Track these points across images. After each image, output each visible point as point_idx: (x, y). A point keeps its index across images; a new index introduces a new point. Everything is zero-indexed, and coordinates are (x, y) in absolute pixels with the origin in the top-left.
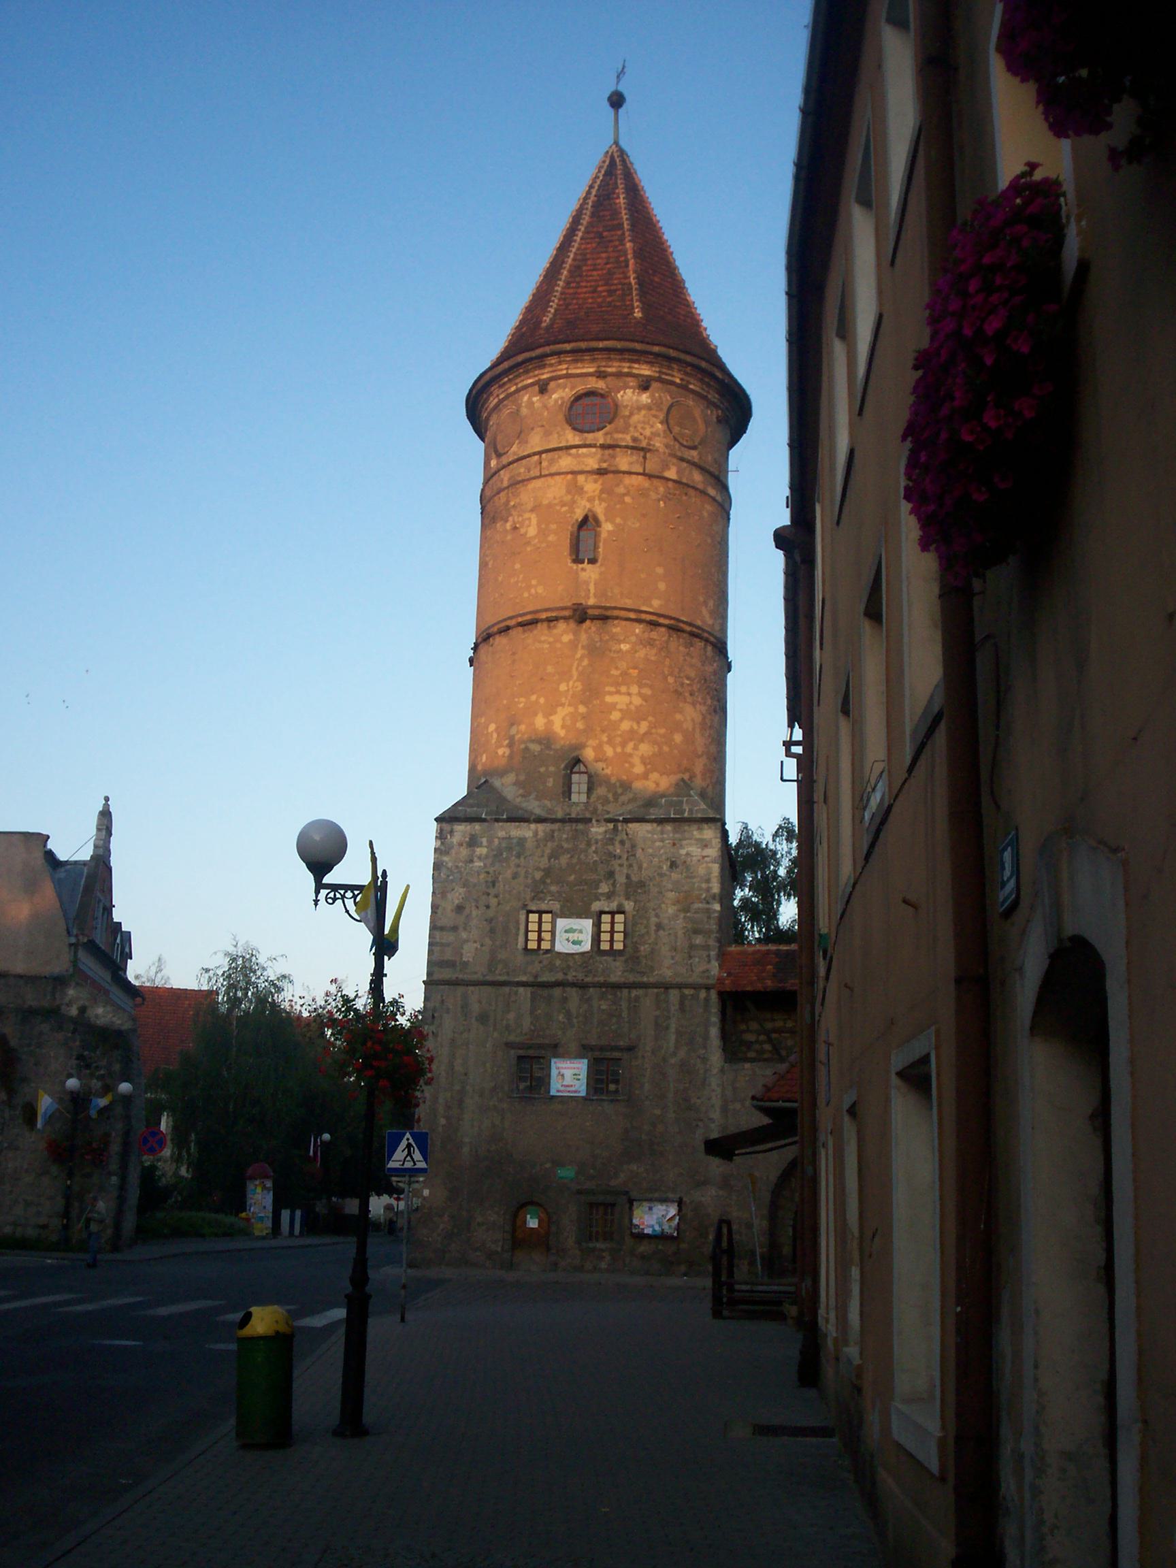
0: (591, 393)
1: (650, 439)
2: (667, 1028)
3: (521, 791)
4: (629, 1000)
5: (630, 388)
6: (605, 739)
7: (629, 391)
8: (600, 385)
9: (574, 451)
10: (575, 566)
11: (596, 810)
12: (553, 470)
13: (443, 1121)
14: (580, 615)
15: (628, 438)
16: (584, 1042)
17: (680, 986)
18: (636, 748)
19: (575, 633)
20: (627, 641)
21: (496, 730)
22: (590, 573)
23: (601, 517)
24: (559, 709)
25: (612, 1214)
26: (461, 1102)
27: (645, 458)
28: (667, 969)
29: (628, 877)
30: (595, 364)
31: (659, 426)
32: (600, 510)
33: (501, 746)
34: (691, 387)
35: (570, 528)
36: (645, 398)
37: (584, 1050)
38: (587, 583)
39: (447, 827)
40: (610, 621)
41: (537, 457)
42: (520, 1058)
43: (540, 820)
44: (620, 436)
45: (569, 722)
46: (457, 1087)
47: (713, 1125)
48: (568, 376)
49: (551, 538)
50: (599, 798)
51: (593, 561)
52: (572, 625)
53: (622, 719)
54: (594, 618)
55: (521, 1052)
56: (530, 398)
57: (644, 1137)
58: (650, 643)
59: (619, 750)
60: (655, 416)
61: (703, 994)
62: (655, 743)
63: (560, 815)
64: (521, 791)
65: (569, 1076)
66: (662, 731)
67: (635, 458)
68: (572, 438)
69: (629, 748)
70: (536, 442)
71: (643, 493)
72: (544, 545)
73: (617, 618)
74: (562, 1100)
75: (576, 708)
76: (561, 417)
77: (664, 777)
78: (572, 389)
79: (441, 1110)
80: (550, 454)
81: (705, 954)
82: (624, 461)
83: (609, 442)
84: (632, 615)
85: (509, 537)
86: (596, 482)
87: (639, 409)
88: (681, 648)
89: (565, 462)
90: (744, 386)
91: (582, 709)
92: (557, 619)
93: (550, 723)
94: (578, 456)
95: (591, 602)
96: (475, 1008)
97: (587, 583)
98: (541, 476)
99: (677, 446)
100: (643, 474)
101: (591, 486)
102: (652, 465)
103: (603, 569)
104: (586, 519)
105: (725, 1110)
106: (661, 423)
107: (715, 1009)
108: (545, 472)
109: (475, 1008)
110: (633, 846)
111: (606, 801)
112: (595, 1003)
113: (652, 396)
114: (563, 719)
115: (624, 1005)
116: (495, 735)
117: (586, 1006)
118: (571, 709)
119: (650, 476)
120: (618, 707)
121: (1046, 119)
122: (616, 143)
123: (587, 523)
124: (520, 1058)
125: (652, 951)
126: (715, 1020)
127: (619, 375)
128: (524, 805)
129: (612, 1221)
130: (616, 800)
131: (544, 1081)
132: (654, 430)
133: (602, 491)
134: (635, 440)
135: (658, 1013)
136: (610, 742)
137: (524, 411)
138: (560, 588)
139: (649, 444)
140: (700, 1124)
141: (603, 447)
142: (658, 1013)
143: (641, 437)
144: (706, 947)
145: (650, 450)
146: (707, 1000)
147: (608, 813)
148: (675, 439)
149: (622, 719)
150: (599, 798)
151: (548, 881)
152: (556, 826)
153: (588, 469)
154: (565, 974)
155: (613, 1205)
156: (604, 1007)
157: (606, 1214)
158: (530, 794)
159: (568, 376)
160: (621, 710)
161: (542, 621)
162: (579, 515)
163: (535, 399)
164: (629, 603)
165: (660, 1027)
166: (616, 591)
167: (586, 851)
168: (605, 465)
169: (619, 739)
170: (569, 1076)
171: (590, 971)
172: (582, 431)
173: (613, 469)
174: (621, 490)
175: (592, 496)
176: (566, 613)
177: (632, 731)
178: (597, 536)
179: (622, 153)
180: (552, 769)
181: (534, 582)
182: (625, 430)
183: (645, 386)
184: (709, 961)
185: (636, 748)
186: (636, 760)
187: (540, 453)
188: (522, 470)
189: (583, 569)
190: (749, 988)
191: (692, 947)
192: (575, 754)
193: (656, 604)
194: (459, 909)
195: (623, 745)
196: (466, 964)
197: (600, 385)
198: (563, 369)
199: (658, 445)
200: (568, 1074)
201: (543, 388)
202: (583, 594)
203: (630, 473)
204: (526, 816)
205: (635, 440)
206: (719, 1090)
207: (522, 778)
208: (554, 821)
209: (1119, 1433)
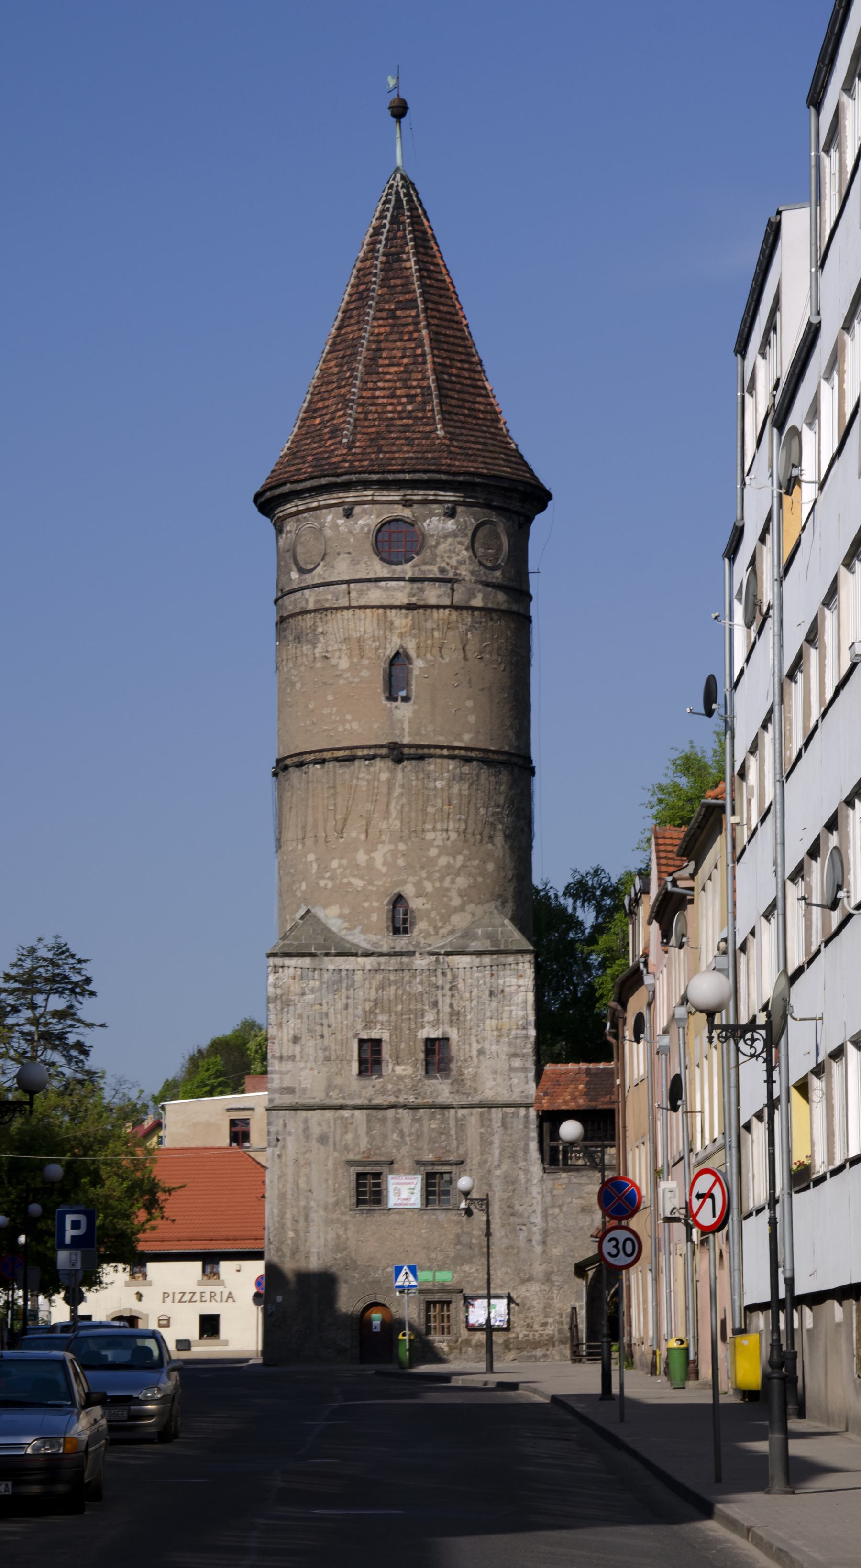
0: (397, 520)
1: (456, 568)
2: (491, 1143)
3: (346, 925)
4: (457, 1120)
5: (435, 515)
6: (424, 875)
7: (435, 519)
8: (407, 513)
9: (383, 584)
10: (389, 704)
11: (418, 943)
13: (291, 1234)
14: (397, 754)
15: (435, 569)
16: (417, 1158)
18: (453, 882)
19: (393, 772)
20: (441, 775)
21: (317, 859)
22: (404, 711)
23: (412, 653)
24: (380, 846)
25: (448, 1311)
26: (307, 1217)
27: (453, 590)
28: (491, 1088)
29: (451, 1006)
30: (402, 493)
31: (465, 553)
32: (411, 646)
33: (323, 878)
34: (494, 504)
35: (383, 665)
36: (450, 524)
38: (401, 721)
40: (427, 761)
41: (344, 586)
42: (360, 1176)
44: (427, 567)
45: (390, 859)
46: (302, 1203)
47: (535, 1229)
48: (374, 502)
49: (365, 673)
50: (421, 932)
51: (406, 699)
52: (390, 763)
53: (439, 855)
54: (410, 758)
55: (360, 1169)
56: (333, 521)
57: (474, 1241)
58: (462, 778)
59: (437, 885)
60: (460, 543)
62: (470, 875)
63: (385, 949)
64: (346, 925)
65: (404, 1191)
66: (476, 863)
67: (442, 590)
68: (380, 569)
69: (447, 883)
70: (342, 569)
71: (449, 626)
72: (356, 680)
73: (431, 756)
74: (401, 1212)
75: (397, 846)
76: (368, 546)
77: (479, 906)
78: (378, 516)
79: (289, 1223)
80: (359, 585)
81: (522, 1075)
82: (433, 594)
83: (418, 575)
84: (445, 752)
85: (318, 665)
86: (406, 616)
87: (445, 537)
88: (492, 779)
89: (375, 595)
90: (534, 661)
91: (402, 847)
92: (374, 757)
93: (371, 860)
94: (387, 589)
95: (406, 740)
96: (316, 1131)
97: (401, 721)
98: (348, 608)
99: (483, 570)
100: (453, 607)
101: (401, 620)
102: (459, 597)
103: (416, 707)
104: (397, 654)
105: (545, 1215)
106: (467, 549)
107: (533, 1125)
108: (354, 603)
109: (316, 1131)
110: (454, 977)
111: (428, 935)
112: (425, 1122)
113: (457, 523)
114: (384, 855)
115: (452, 1123)
116: (315, 866)
117: (417, 1125)
118: (391, 847)
120: (436, 843)
124: (360, 1176)
125: (476, 1075)
128: (349, 938)
129: (448, 1316)
130: (437, 933)
132: (459, 558)
133: (413, 627)
134: (442, 570)
135: (482, 1130)
136: (429, 878)
137: (328, 532)
138: (375, 726)
139: (456, 574)
140: (524, 1228)
141: (412, 580)
142: (482, 1130)
143: (448, 567)
144: (525, 1069)
145: (457, 581)
146: (527, 1116)
147: (430, 945)
148: (481, 564)
149: (439, 855)
150: (421, 932)
151: (378, 1011)
152: (383, 959)
153: (398, 603)
154: (397, 1097)
155: (449, 1303)
156: (433, 1126)
157: (442, 1310)
158: (355, 927)
160: (438, 846)
161: (361, 758)
162: (390, 652)
163: (340, 522)
164: (441, 740)
165: (485, 1142)
166: (430, 728)
167: (410, 982)
168: (414, 600)
169: (437, 875)
171: (419, 1094)
172: (390, 563)
173: (422, 603)
174: (429, 625)
175: (400, 634)
176: (384, 751)
177: (449, 866)
178: (409, 672)
180: (376, 904)
181: (349, 717)
182: (432, 562)
183: (451, 514)
184: (527, 1083)
185: (453, 882)
186: (454, 894)
187: (348, 582)
188: (330, 597)
189: (396, 707)
190: (564, 1108)
191: (512, 1069)
192: (396, 891)
193: (467, 739)
195: (442, 879)
196: (304, 1090)
197: (407, 513)
199: (464, 573)
200: (405, 1194)
202: (397, 732)
203: (438, 607)
204: (353, 951)
205: (442, 570)
206: (539, 1197)
207: (346, 911)
208: (381, 954)
209: (373, 1037)
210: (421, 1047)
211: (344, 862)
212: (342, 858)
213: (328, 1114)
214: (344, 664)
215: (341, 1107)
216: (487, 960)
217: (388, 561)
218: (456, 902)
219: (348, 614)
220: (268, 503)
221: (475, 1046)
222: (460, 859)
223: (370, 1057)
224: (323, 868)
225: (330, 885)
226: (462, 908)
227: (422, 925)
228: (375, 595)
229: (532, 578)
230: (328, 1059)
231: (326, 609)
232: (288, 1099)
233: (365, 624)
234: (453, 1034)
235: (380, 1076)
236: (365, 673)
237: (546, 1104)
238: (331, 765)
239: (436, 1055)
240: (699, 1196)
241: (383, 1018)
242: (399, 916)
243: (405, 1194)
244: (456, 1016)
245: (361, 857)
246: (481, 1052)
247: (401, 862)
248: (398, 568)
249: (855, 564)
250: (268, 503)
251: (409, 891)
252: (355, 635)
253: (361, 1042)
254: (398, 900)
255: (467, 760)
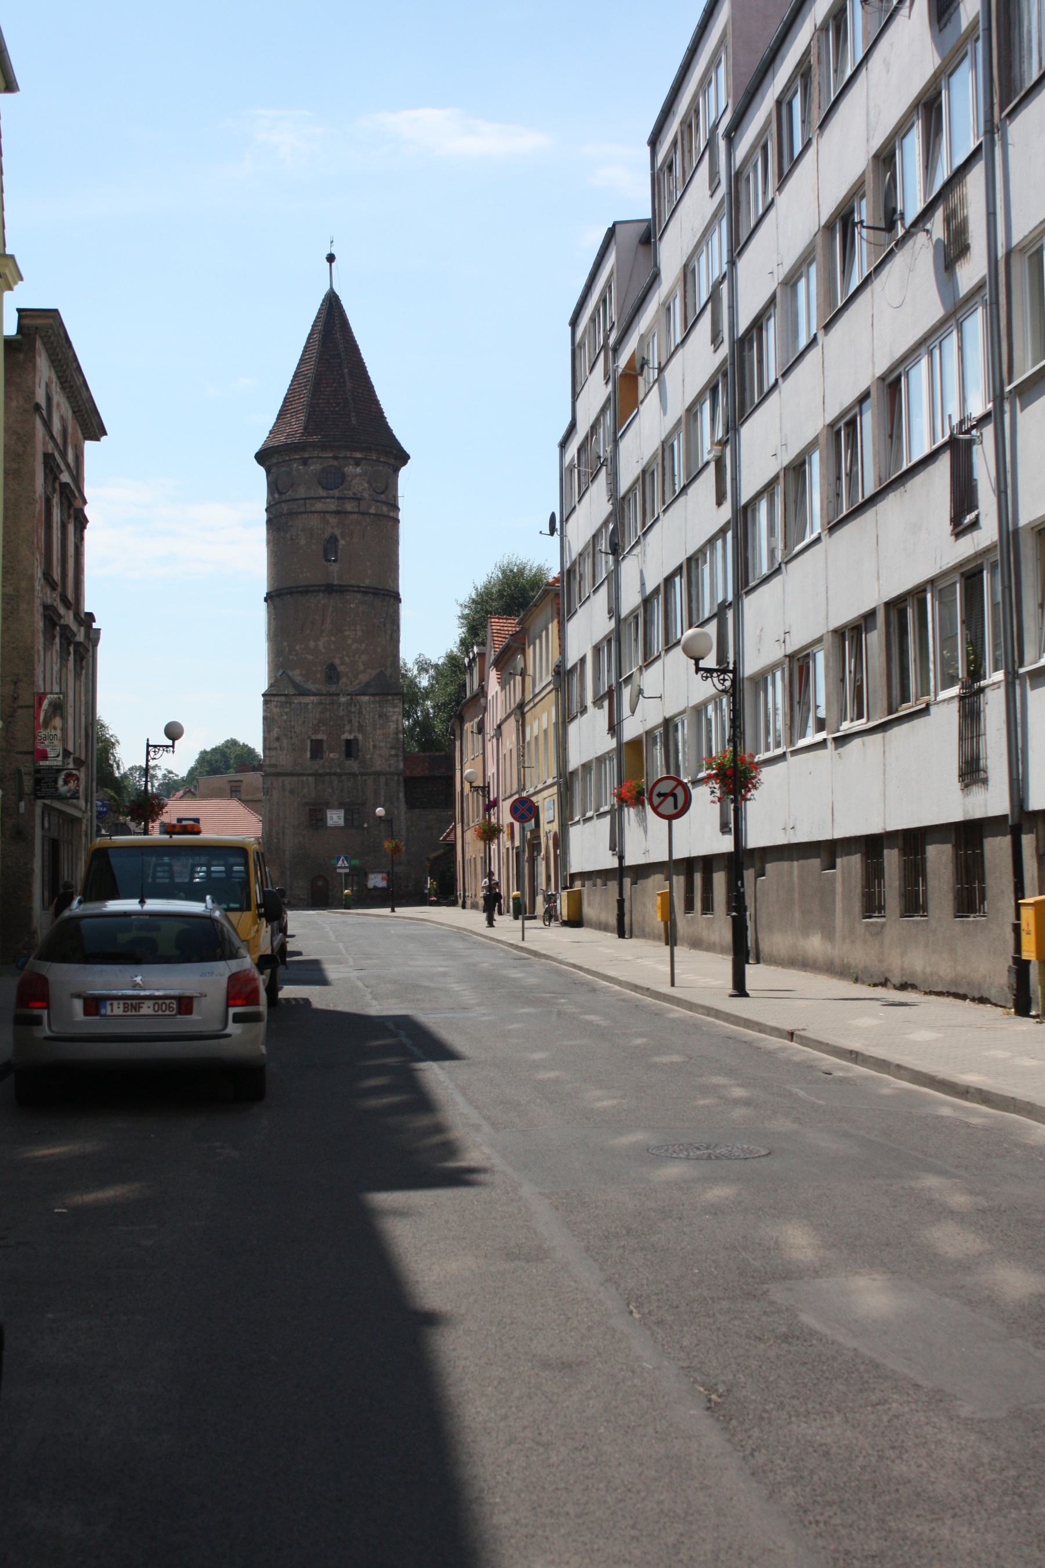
8: (336, 463)
12: (313, 509)
14: (330, 589)
17: (385, 774)
22: (334, 568)
23: (339, 537)
28: (379, 764)
32: (337, 532)
36: (359, 470)
37: (341, 805)
39: (268, 698)
42: (310, 810)
43: (314, 695)
46: (281, 824)
48: (318, 457)
61: (396, 778)
63: (324, 692)
65: (335, 818)
68: (322, 492)
70: (302, 492)
82: (349, 506)
89: (319, 506)
91: (333, 639)
92: (319, 591)
95: (336, 582)
98: (305, 513)
101: (333, 520)
119: (363, 514)
121: (295, 999)
122: (331, 288)
123: (333, 540)
126: (402, 789)
127: (345, 458)
131: (324, 820)
137: (295, 473)
141: (339, 498)
144: (396, 755)
146: (398, 780)
159: (318, 457)
162: (327, 535)
170: (335, 818)
179: (334, 293)
186: (360, 664)
187: (305, 499)
193: (367, 582)
194: (278, 739)
198: (316, 453)
200: (335, 817)
201: (305, 462)
205: (355, 494)
210: (344, 743)
213: (295, 779)
214: (303, 542)
215: (302, 775)
216: (377, 698)
217: (325, 488)
218: (361, 668)
219: (304, 516)
221: (372, 743)
222: (363, 645)
223: (317, 750)
226: (364, 671)
227: (344, 680)
228: (319, 506)
229: (400, 500)
230: (294, 750)
232: (273, 770)
233: (314, 521)
234: (360, 737)
235: (322, 758)
236: (314, 547)
237: (408, 773)
239: (350, 749)
240: (659, 795)
241: (323, 728)
242: (332, 674)
243: (335, 817)
244: (361, 728)
245: (312, 644)
246: (374, 746)
247: (332, 647)
248: (331, 492)
251: (337, 661)
253: (312, 741)
254: (332, 667)
255: (365, 593)
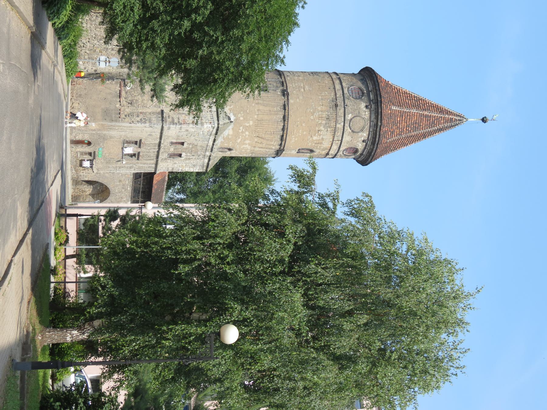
21: (250, 126)
70: (347, 138)
98: (333, 140)
116: (248, 125)
128: (220, 138)
158: (224, 139)
211: (247, 137)
212: (249, 136)
214: (315, 138)
219: (331, 140)
220: (368, 74)
224: (246, 128)
225: (240, 131)
231: (335, 133)
236: (310, 144)
238: (282, 133)
249: (131, 147)
250: (368, 74)
252: (323, 142)
